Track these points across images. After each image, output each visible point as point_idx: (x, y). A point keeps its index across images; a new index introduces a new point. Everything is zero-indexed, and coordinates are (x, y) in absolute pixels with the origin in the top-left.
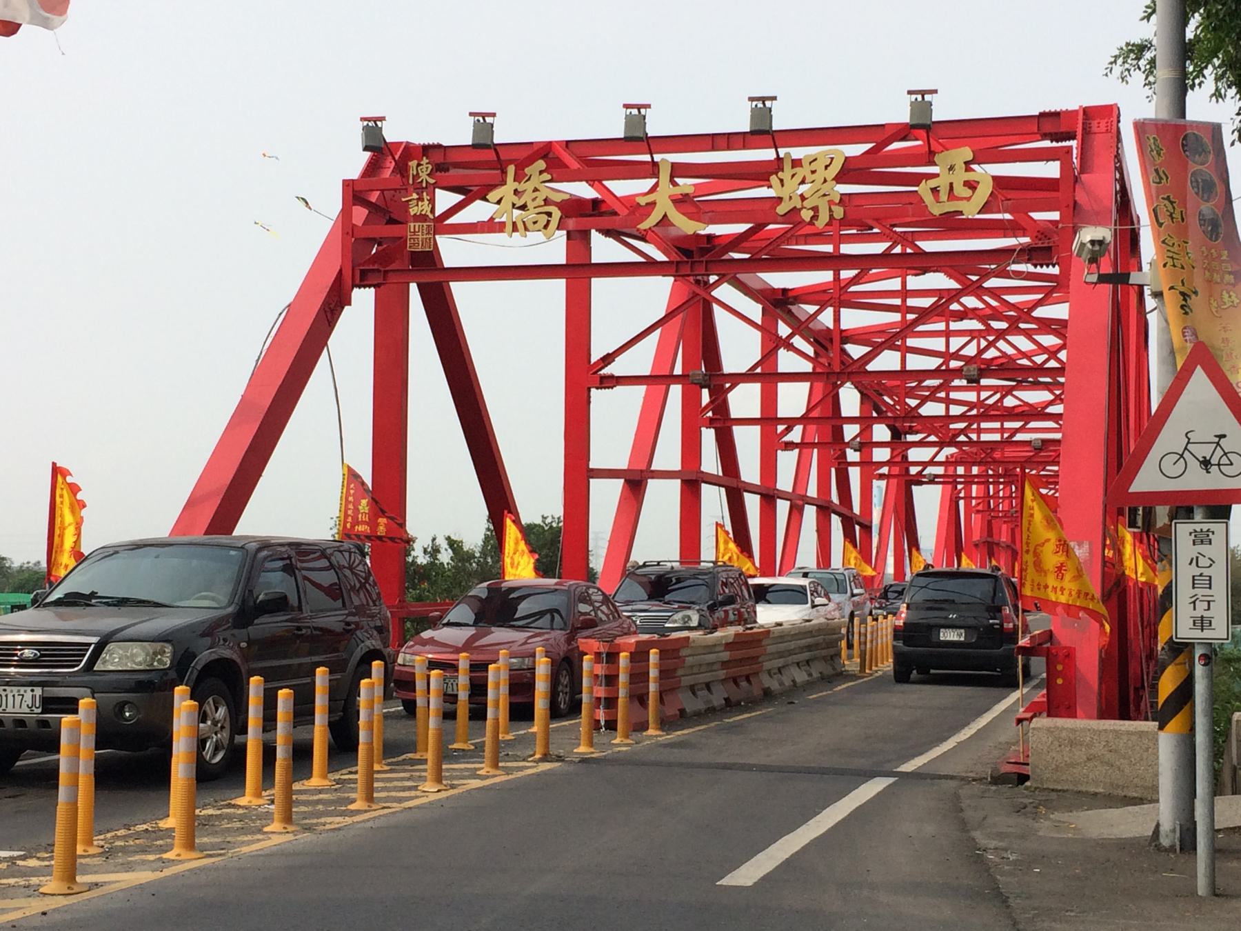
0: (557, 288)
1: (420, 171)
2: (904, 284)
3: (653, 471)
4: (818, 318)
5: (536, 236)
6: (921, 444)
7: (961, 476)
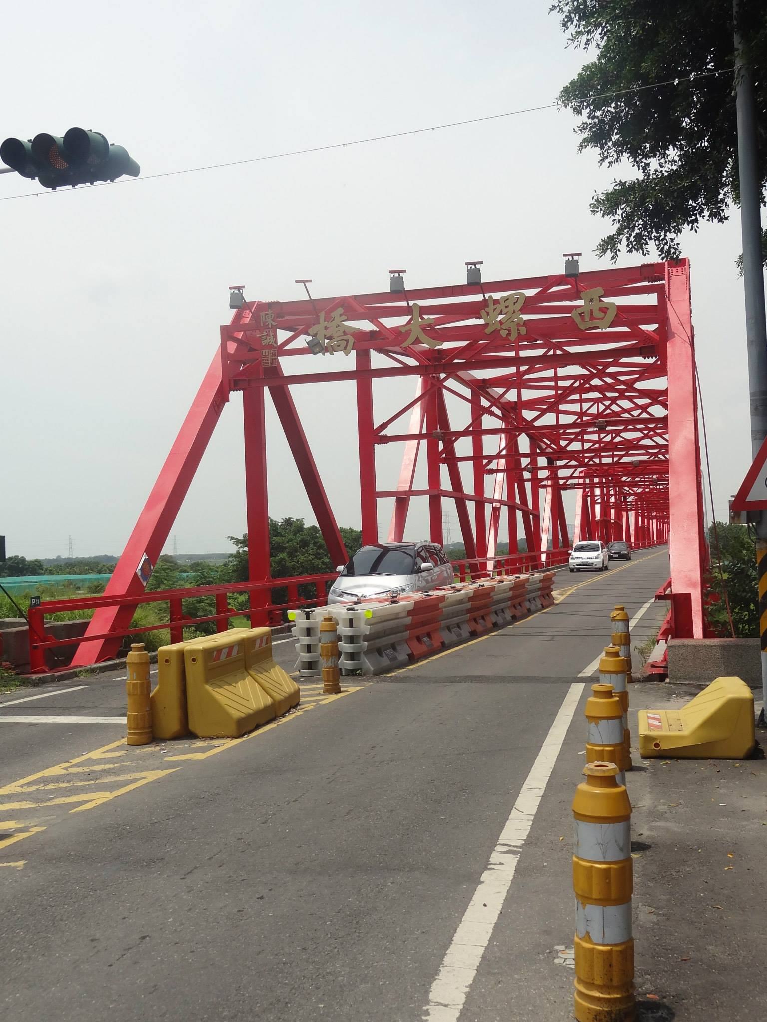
0: (352, 384)
1: (267, 318)
2: (556, 373)
3: (413, 491)
4: (505, 396)
5: (339, 355)
6: (566, 466)
7: (588, 484)
